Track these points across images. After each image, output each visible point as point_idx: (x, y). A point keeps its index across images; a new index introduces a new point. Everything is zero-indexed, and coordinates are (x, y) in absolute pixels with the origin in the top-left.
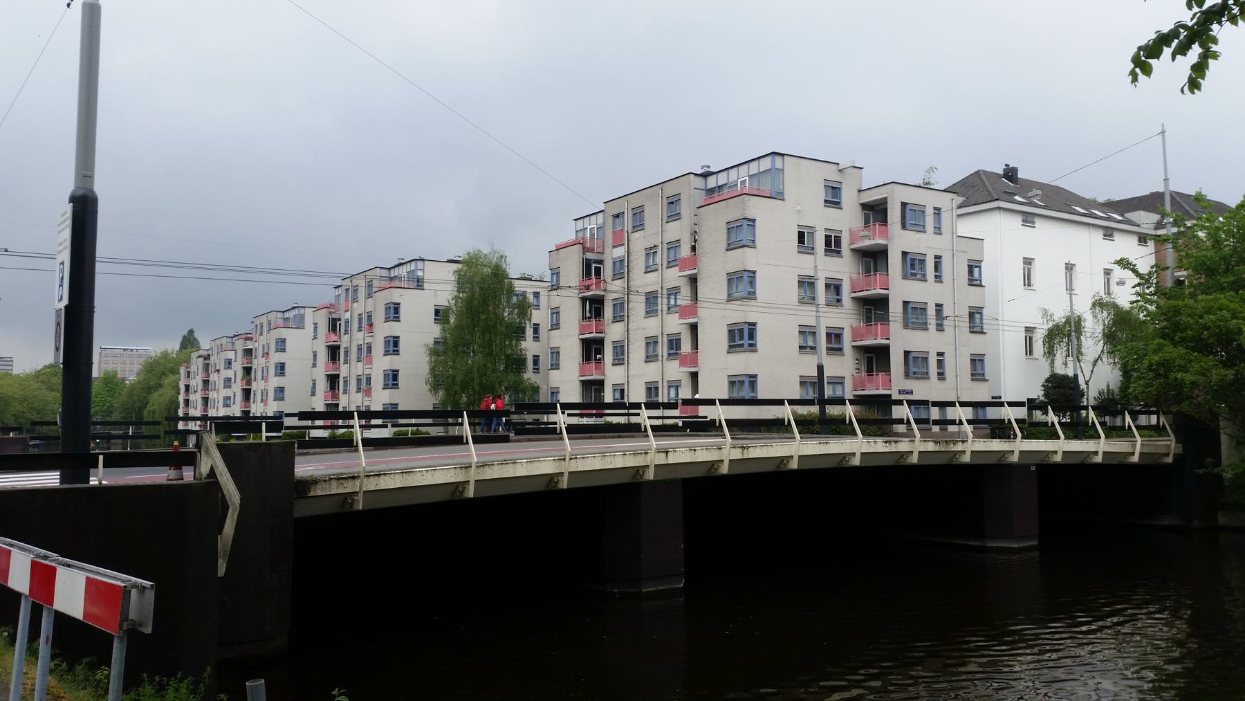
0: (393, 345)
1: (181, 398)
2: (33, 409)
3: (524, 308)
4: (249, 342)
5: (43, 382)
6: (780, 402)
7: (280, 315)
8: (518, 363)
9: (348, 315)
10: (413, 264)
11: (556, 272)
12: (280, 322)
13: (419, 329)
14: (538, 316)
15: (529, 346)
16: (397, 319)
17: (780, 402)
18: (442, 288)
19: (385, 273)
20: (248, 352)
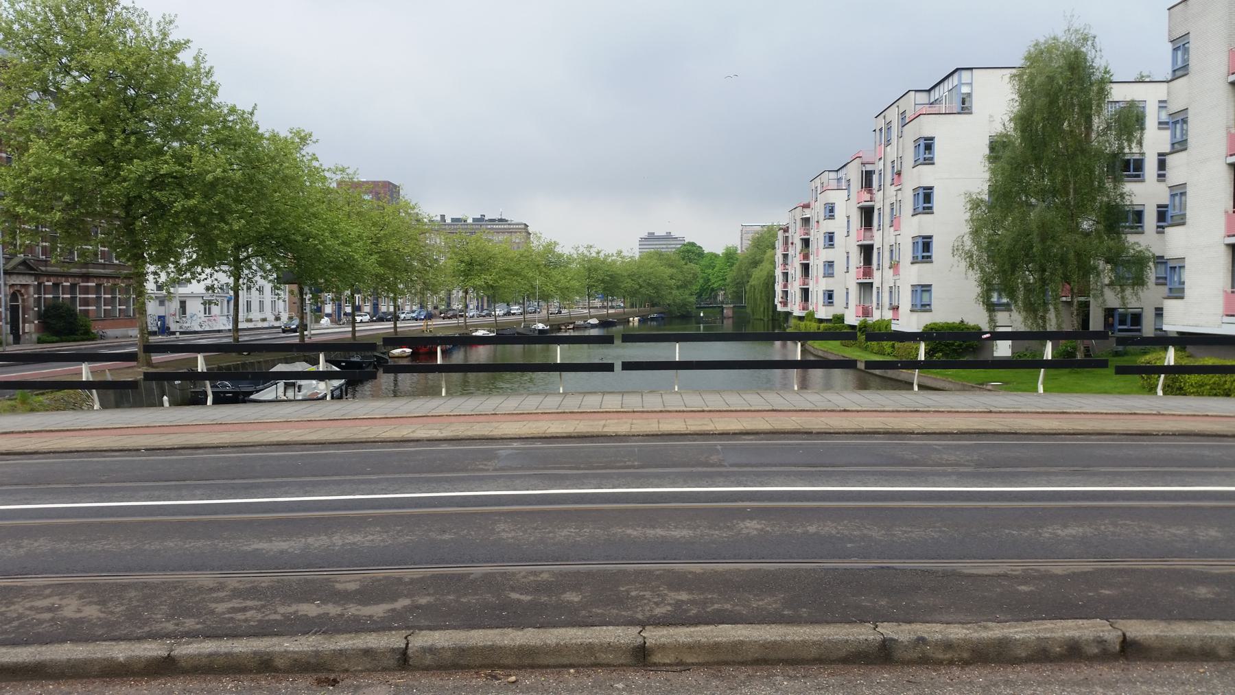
0: (926, 197)
1: (778, 273)
2: (649, 284)
3: (1130, 121)
4: (806, 210)
5: (456, 253)
6: (628, 366)
7: (833, 175)
8: (1123, 218)
9: (881, 165)
10: (956, 76)
11: (1180, 44)
12: (834, 184)
13: (963, 169)
14: (1154, 141)
15: (1144, 193)
16: (929, 161)
17: (628, 366)
18: (997, 104)
19: (922, 98)
20: (806, 221)
